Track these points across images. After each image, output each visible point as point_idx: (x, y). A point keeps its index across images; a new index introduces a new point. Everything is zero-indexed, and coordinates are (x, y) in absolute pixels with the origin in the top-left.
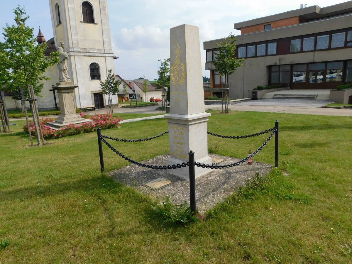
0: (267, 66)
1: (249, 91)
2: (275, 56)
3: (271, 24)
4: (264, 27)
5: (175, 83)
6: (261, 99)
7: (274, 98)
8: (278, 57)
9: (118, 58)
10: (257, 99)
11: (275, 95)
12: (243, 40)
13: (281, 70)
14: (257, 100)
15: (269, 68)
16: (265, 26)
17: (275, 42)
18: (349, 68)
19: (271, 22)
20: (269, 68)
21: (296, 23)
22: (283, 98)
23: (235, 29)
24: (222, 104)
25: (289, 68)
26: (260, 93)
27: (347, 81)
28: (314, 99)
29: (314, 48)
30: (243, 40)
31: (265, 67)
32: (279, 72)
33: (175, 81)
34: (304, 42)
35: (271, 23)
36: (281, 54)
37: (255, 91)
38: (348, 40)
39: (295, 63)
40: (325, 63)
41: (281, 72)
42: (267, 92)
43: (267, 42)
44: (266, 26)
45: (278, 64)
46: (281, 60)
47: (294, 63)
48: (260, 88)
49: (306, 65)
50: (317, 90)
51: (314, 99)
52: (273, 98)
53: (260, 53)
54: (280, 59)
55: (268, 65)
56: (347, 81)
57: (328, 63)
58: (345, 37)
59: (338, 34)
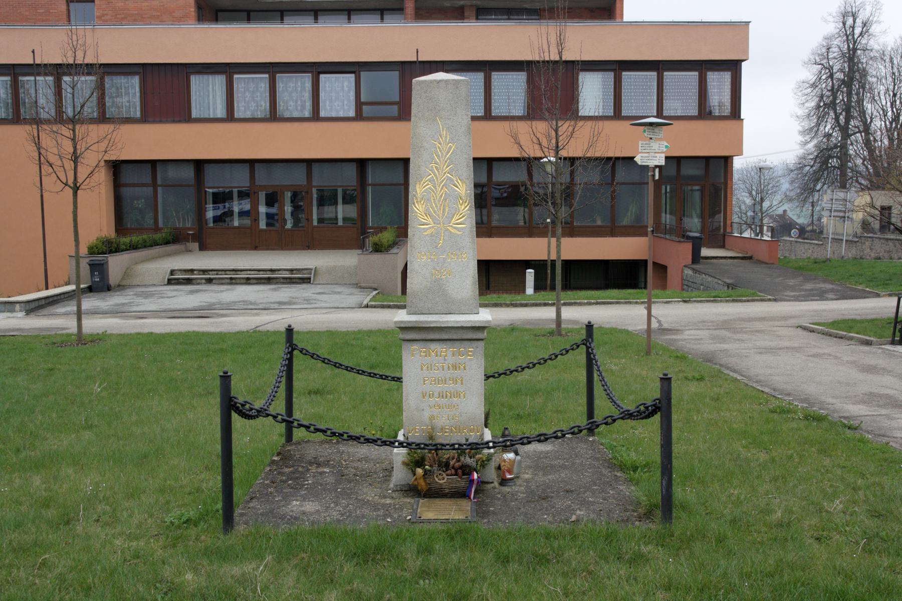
1: (70, 256)
5: (430, 228)
6: (121, 287)
9: (417, 50)
10: (109, 289)
11: (172, 272)
12: (33, 52)
13: (159, 182)
14: (108, 293)
18: (372, 185)
25: (189, 174)
26: (116, 264)
28: (310, 282)
29: (580, 80)
30: (33, 52)
32: (154, 184)
34: (280, 86)
38: (363, 100)
41: (160, 186)
51: (310, 282)
52: (170, 282)
59: (253, 78)
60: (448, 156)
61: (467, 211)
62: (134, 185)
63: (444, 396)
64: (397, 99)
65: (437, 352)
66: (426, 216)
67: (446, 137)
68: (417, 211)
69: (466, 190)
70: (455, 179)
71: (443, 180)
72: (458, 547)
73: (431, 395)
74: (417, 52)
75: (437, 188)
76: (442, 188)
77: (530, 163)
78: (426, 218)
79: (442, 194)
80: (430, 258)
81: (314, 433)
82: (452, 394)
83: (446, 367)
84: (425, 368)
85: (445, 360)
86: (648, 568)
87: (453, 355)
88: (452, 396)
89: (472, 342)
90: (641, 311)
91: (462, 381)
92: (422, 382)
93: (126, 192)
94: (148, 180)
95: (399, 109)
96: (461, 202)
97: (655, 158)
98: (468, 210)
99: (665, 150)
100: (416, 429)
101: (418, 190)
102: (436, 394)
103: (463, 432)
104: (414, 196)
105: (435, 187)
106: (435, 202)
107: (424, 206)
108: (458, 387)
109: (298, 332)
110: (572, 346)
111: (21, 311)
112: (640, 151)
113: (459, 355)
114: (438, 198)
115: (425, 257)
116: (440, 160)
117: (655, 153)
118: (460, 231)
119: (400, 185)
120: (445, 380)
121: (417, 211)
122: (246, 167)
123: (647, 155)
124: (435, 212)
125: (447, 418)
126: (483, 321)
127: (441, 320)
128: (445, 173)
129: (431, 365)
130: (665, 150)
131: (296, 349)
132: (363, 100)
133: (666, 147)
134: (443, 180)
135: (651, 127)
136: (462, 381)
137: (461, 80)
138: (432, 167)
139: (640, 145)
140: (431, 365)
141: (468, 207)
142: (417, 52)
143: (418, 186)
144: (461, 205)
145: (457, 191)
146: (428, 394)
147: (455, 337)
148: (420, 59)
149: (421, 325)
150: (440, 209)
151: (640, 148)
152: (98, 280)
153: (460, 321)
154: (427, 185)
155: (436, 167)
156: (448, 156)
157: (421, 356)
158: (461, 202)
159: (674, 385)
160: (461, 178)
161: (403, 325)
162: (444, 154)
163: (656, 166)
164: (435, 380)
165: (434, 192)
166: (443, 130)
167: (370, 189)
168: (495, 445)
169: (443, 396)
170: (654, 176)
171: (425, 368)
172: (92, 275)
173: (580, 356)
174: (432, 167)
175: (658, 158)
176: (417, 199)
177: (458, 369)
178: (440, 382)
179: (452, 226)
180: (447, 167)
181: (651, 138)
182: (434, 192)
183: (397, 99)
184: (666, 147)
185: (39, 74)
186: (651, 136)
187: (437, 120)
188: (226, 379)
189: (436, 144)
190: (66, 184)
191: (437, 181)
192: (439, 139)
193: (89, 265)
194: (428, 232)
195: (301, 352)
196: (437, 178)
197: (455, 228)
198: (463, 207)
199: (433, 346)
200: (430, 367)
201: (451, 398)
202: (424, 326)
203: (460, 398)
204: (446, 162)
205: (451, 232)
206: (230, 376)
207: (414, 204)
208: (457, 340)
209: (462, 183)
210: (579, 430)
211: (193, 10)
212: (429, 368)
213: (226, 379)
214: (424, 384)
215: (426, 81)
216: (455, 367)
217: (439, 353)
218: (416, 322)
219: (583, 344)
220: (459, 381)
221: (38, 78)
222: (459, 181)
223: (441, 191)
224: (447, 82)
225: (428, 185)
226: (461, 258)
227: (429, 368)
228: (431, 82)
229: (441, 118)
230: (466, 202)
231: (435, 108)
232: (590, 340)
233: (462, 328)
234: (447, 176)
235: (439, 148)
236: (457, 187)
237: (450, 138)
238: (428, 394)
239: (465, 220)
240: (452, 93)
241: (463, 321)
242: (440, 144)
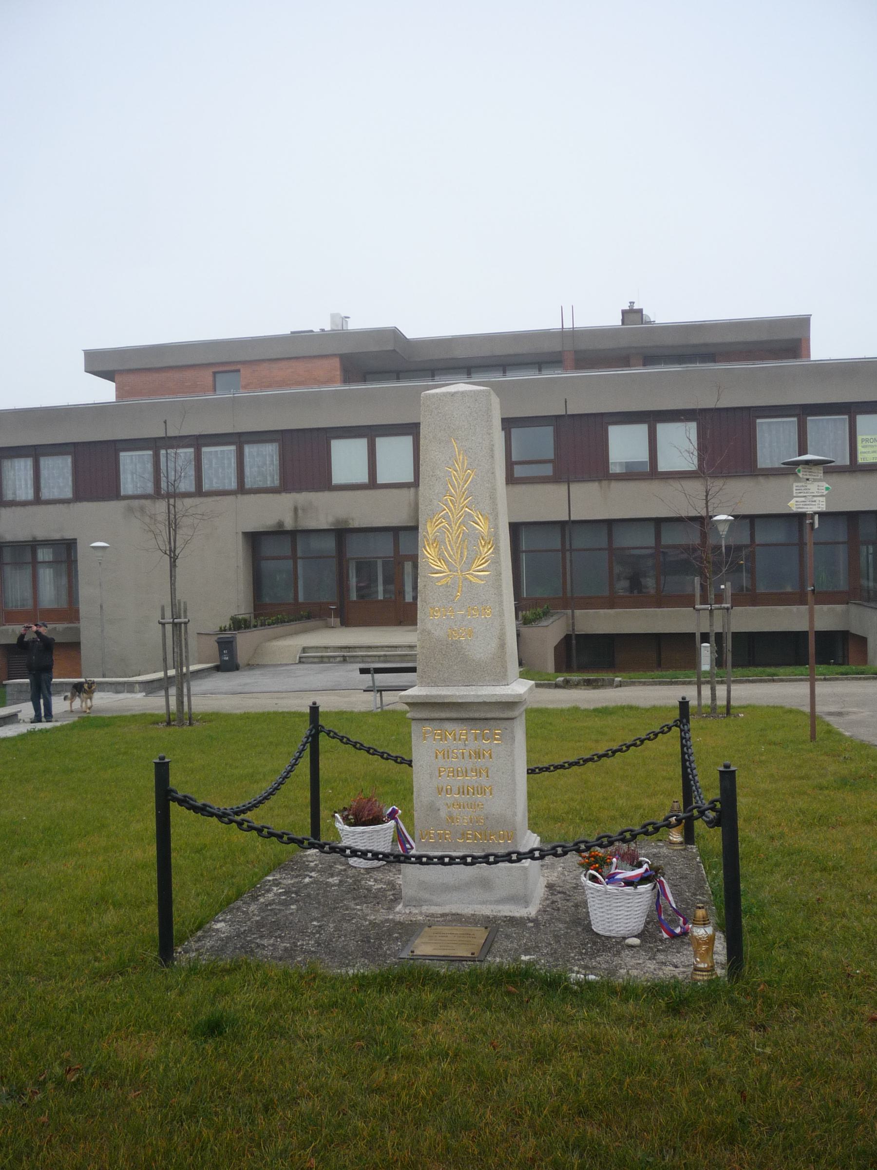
0: (246, 535)
2: (277, 497)
3: (239, 371)
4: (211, 378)
5: (445, 577)
6: (250, 666)
7: (303, 663)
8: (288, 500)
11: (304, 650)
12: (165, 422)
13: (299, 554)
15: (254, 539)
16: (215, 373)
17: (26, 456)
18: (525, 552)
19: (244, 363)
20: (254, 539)
21: (330, 381)
22: (316, 660)
23: (86, 371)
24: (163, 693)
25: (329, 544)
26: (244, 641)
27: (381, 597)
30: (165, 422)
31: (240, 537)
32: (294, 558)
33: (443, 572)
35: (239, 367)
36: (300, 490)
37: (228, 635)
38: (514, 459)
39: (355, 524)
40: (748, 521)
41: (300, 558)
42: (276, 638)
43: (240, 440)
44: (218, 376)
45: (289, 525)
46: (300, 512)
47: (351, 526)
48: (239, 624)
49: (651, 530)
50: (385, 628)
53: (215, 480)
54: (296, 510)
55: (250, 529)
56: (381, 597)
57: (402, 534)
58: (119, 466)
60: (466, 486)
61: (490, 554)
62: (274, 558)
63: (466, 792)
64: (551, 455)
65: (455, 735)
66: (440, 562)
67: (463, 462)
68: (429, 556)
69: (489, 528)
70: (475, 514)
71: (461, 517)
72: (93, 1065)
73: (449, 791)
74: (566, 402)
75: (453, 526)
76: (459, 527)
77: (703, 522)
78: (439, 564)
79: (460, 533)
80: (445, 615)
81: (267, 838)
82: (476, 789)
83: (466, 755)
84: (440, 756)
85: (465, 745)
86: (724, 1036)
87: (476, 739)
88: (476, 792)
89: (498, 722)
90: (803, 689)
91: (487, 772)
92: (437, 773)
93: (268, 566)
94: (289, 553)
95: (554, 467)
96: (483, 543)
97: (814, 503)
98: (492, 553)
99: (825, 492)
100: (430, 833)
101: (429, 529)
102: (455, 789)
103: (491, 839)
104: (425, 537)
105: (450, 525)
106: (450, 544)
107: (437, 550)
108: (483, 780)
109: (328, 714)
110: (661, 728)
111: (140, 692)
112: (795, 495)
113: (484, 739)
114: (454, 538)
115: (439, 614)
116: (456, 492)
117: (814, 496)
118: (482, 581)
119: (558, 551)
120: (466, 772)
121: (429, 556)
122: (390, 536)
123: (803, 499)
124: (450, 556)
125: (469, 821)
126: (511, 695)
127: (457, 694)
128: (463, 507)
129: (448, 752)
130: (825, 492)
131: (322, 731)
132: (514, 459)
133: (827, 489)
134: (461, 517)
135: (807, 466)
136: (487, 772)
137: (481, 390)
138: (446, 500)
139: (795, 488)
140: (448, 752)
141: (492, 549)
142: (566, 402)
143: (428, 525)
144: (484, 547)
145: (477, 529)
146: (444, 789)
147: (476, 715)
148: (569, 413)
149: (433, 701)
150: (457, 552)
151: (795, 491)
152: (227, 658)
153: (481, 696)
154: (440, 523)
155: (451, 500)
156: (466, 486)
157: (435, 740)
158: (483, 543)
159: (739, 780)
160: (482, 513)
161: (409, 701)
162: (462, 484)
163: (815, 513)
164: (453, 770)
165: (448, 531)
166: (459, 455)
167: (524, 556)
168: (497, 859)
169: (463, 792)
170: (812, 524)
171: (440, 756)
172: (221, 654)
173: (670, 743)
174: (446, 500)
175: (817, 502)
176: (428, 540)
177: (482, 757)
178: (460, 774)
179: (472, 574)
180: (465, 500)
181: (808, 479)
182: (448, 531)
183: (552, 457)
184: (827, 489)
185: (178, 447)
186: (808, 477)
187: (451, 441)
188: (162, 769)
189: (450, 472)
190: (166, 554)
191: (453, 517)
192: (454, 465)
193: (218, 643)
194: (443, 582)
195: (328, 734)
196: (452, 514)
197: (477, 576)
198: (486, 550)
199: (449, 726)
200: (446, 755)
201: (474, 794)
202: (436, 701)
203: (485, 794)
204: (464, 493)
205: (471, 581)
206: (168, 762)
207: (425, 547)
208: (427, 719)
209: (484, 519)
210: (609, 842)
211: (338, 373)
212: (446, 756)
213: (162, 769)
214: (440, 776)
215: (437, 394)
216: (478, 755)
217: (457, 737)
218: (427, 696)
219: (676, 726)
220: (484, 773)
221: (169, 451)
222: (480, 517)
223: (458, 530)
224: (463, 393)
225: (442, 522)
226: (484, 615)
227: (446, 756)
228: (445, 394)
229: (456, 439)
230: (489, 543)
231: (449, 427)
232: (685, 721)
233: (485, 703)
234: (465, 511)
235: (455, 477)
236: (479, 525)
237: (468, 464)
238: (444, 789)
239: (488, 566)
240: (469, 407)
241: (485, 695)
242: (456, 471)
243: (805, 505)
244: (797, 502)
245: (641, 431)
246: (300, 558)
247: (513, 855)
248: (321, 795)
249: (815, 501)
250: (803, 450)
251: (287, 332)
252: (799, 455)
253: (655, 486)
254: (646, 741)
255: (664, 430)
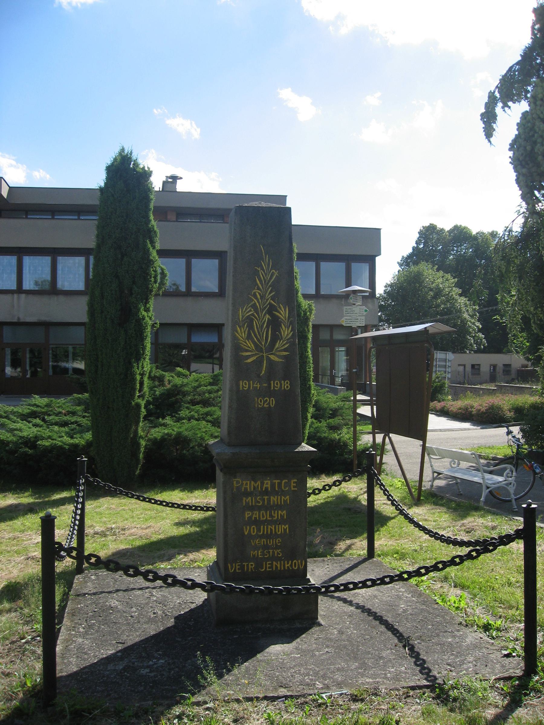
49: (185, 331)
99: (365, 313)
151: (345, 312)
184: (366, 311)
243: (351, 321)
244: (346, 319)
245: (47, 260)
246: (189, 338)
247: (169, 579)
248: (511, 544)
249: (358, 319)
250: (348, 284)
251: (514, 137)
252: (346, 288)
253: (190, 301)
254: (321, 488)
255: (63, 262)
